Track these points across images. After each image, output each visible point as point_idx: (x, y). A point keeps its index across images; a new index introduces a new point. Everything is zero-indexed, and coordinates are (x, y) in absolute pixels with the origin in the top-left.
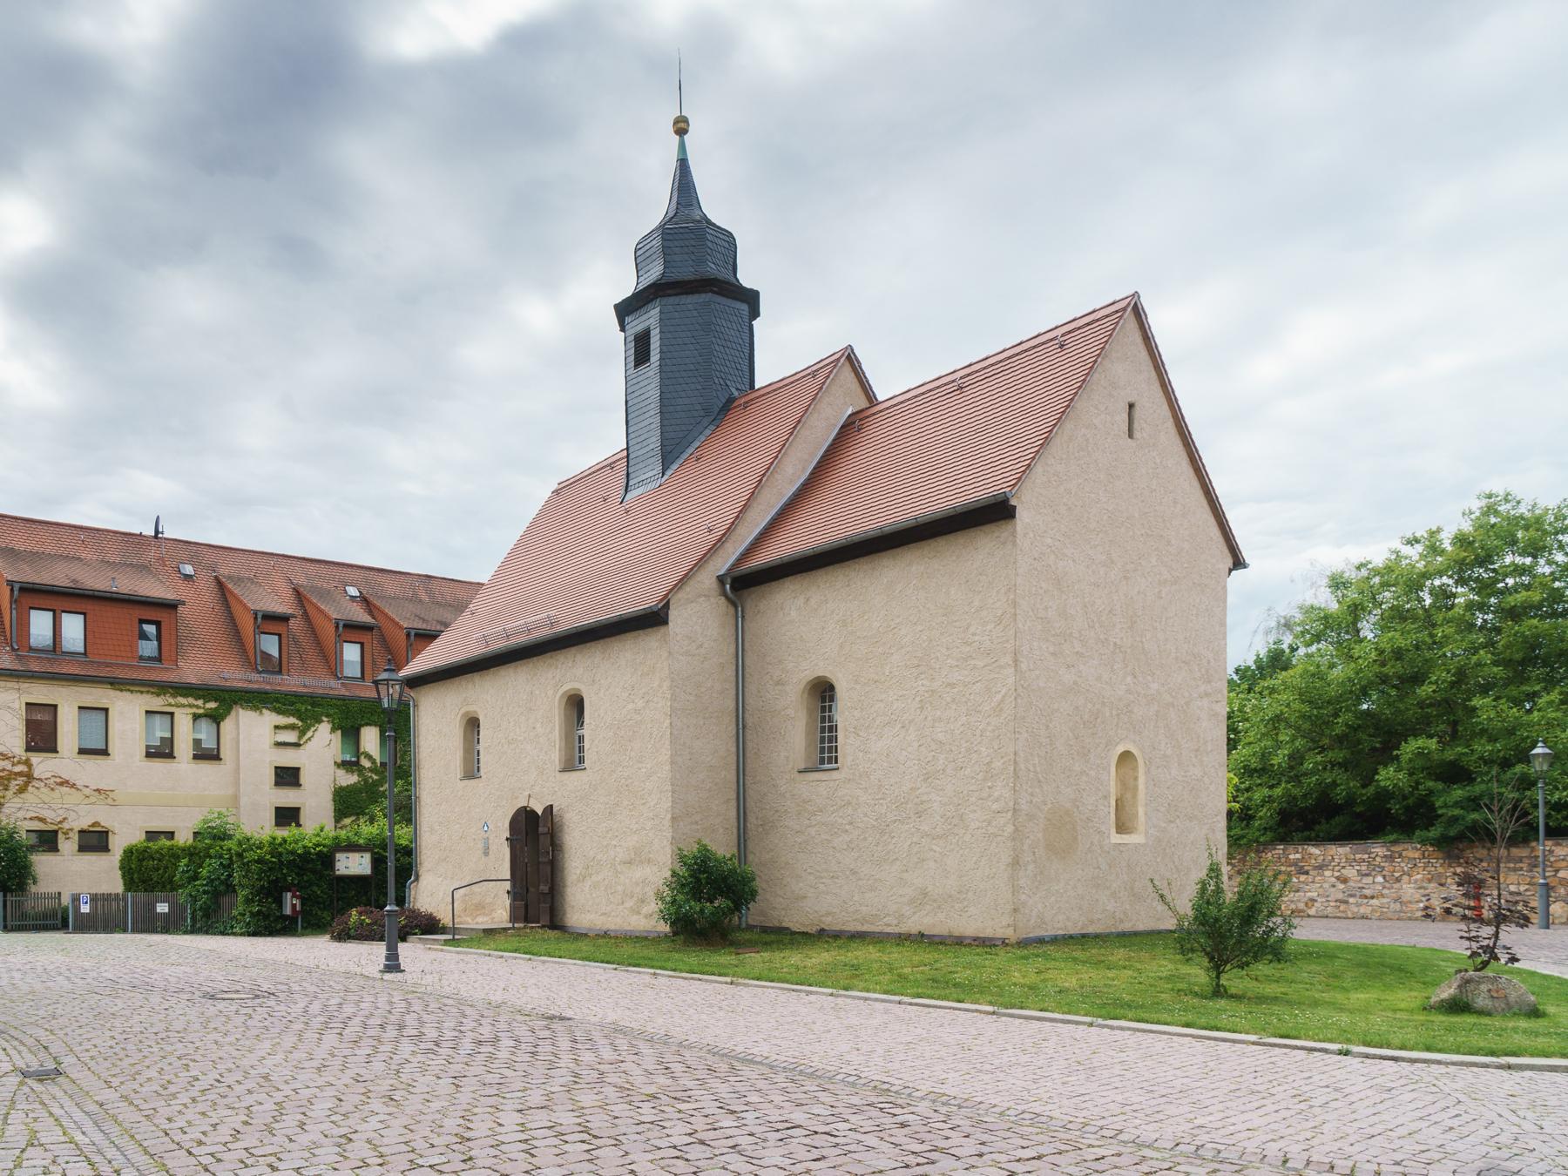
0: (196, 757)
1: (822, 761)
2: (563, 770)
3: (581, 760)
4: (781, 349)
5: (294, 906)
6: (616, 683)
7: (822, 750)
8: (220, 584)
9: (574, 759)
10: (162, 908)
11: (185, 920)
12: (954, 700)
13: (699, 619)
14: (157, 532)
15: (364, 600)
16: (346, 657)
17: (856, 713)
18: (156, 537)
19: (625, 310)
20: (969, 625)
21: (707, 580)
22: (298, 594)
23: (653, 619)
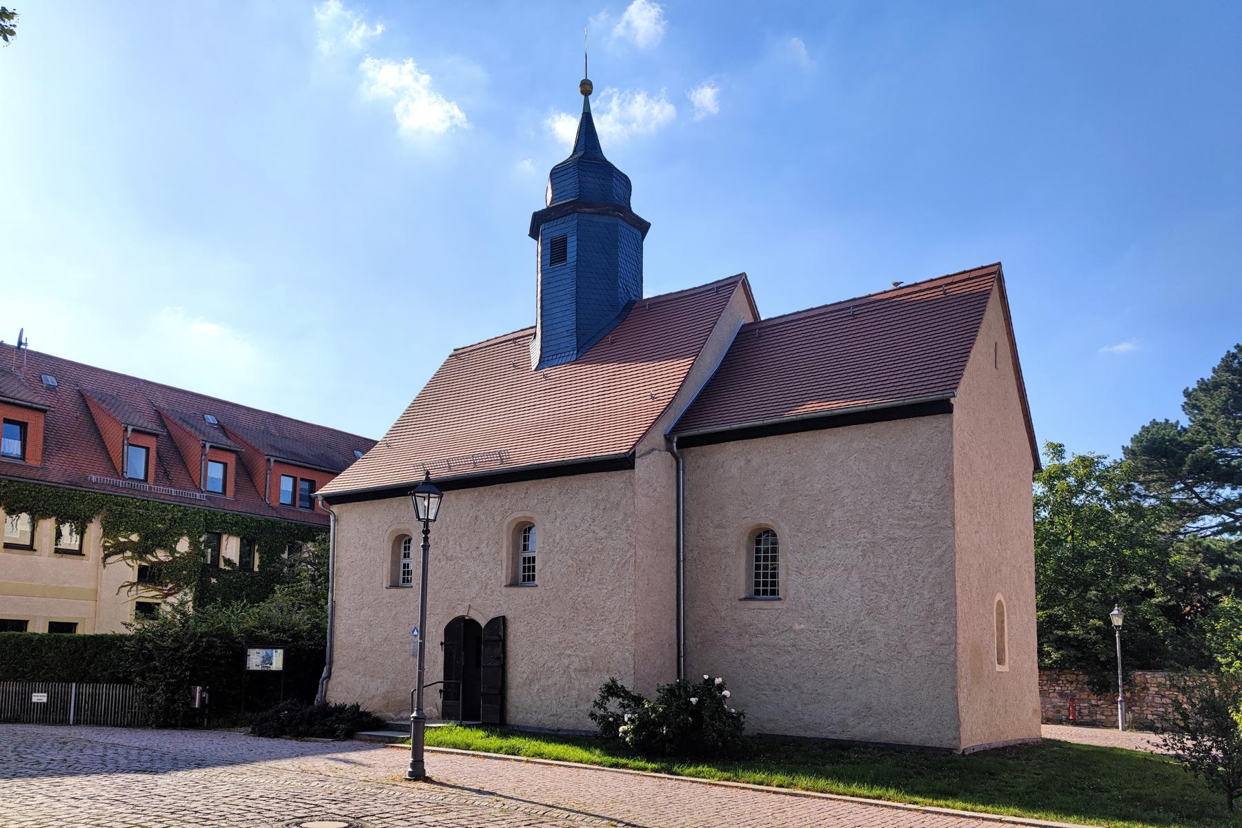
0: (57, 551)
1: (757, 592)
2: (513, 584)
3: (406, 580)
4: (664, 271)
5: (202, 699)
6: (559, 516)
7: (757, 584)
8: (81, 395)
9: (524, 574)
10: (40, 698)
11: (1121, 637)
12: (895, 552)
13: (654, 470)
14: (20, 343)
15: (222, 428)
16: (210, 474)
17: (798, 555)
18: (19, 347)
19: (539, 223)
20: (910, 493)
21: (658, 438)
22: (159, 414)
23: (623, 463)
